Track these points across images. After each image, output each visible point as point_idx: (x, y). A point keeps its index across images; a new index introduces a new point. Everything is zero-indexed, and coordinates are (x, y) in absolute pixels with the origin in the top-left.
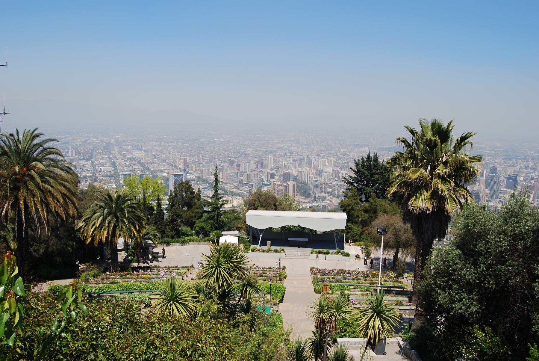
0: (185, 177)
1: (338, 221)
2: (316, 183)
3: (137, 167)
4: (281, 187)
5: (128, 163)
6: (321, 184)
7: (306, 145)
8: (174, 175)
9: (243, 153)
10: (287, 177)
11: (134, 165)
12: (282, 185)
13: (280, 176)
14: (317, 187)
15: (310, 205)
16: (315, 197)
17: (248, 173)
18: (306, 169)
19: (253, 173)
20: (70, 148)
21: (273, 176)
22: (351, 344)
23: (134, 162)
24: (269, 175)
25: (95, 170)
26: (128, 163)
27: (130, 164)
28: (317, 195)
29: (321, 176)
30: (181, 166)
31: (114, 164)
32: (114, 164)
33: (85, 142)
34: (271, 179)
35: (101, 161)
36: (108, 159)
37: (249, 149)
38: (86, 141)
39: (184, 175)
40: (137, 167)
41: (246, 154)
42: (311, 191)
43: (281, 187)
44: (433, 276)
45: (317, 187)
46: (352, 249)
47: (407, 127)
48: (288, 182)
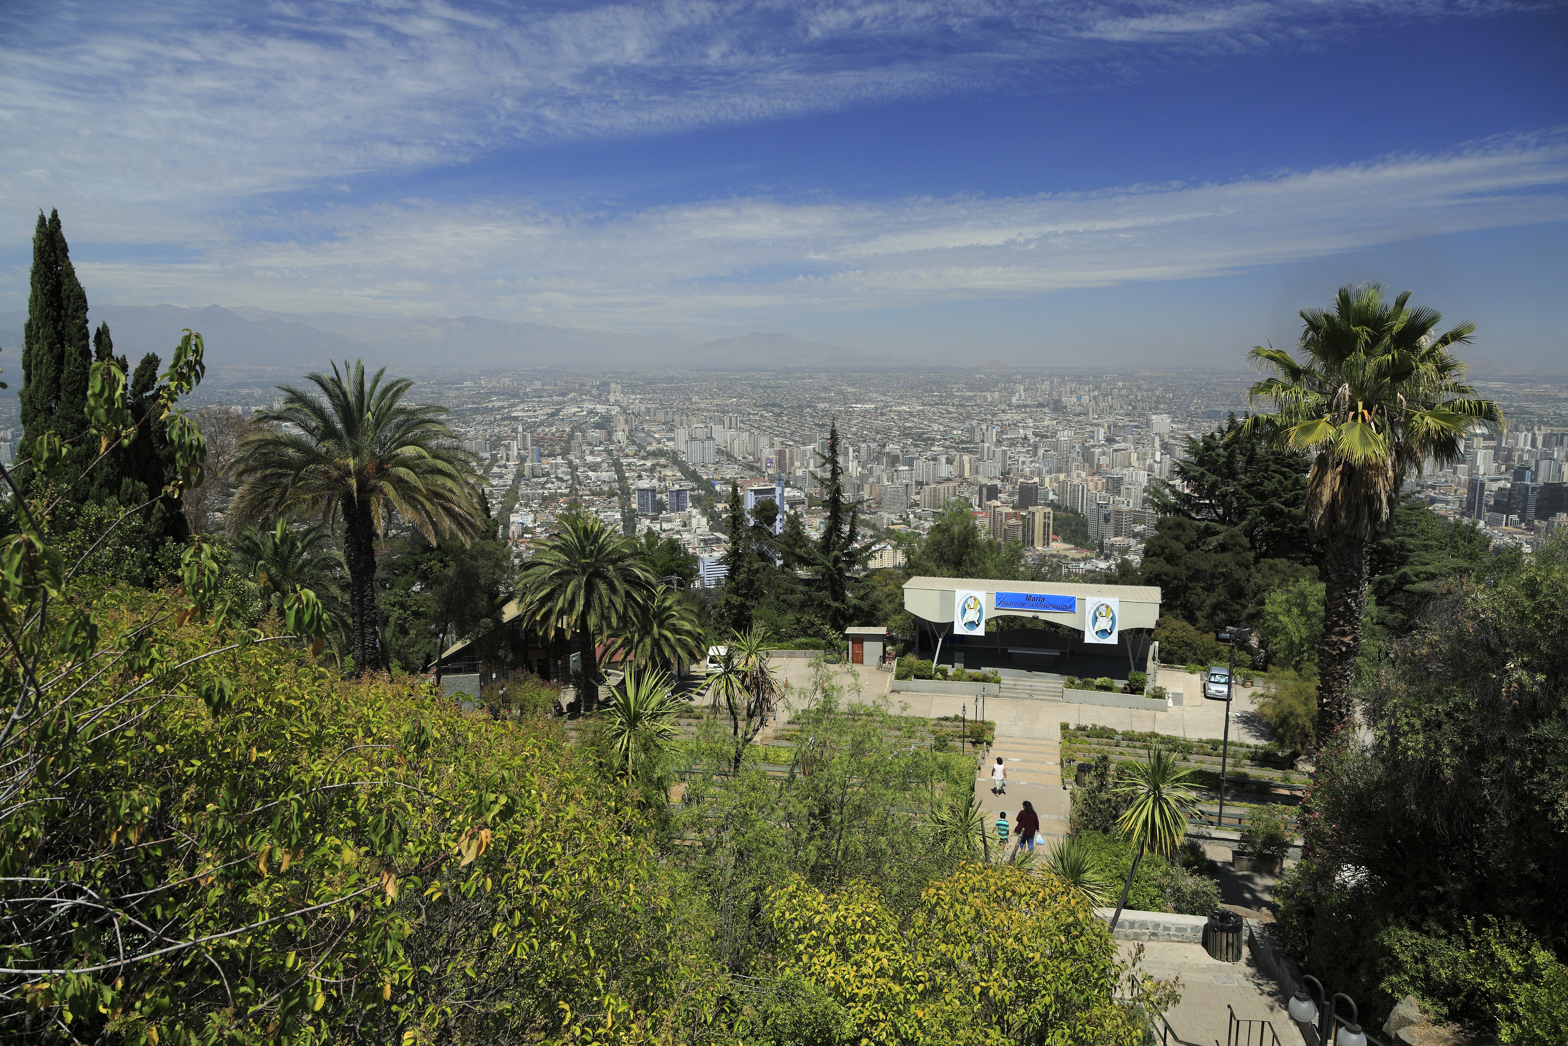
0: (782, 495)
1: (1141, 607)
2: (1104, 511)
3: (669, 473)
4: (1013, 521)
5: (649, 463)
6: (1119, 513)
7: (1079, 415)
8: (756, 492)
9: (919, 437)
10: (1028, 496)
11: (665, 466)
12: (1015, 515)
13: (1011, 494)
14: (1107, 519)
15: (1088, 566)
16: (1101, 546)
17: (933, 486)
18: (1079, 476)
19: (946, 485)
20: (520, 429)
21: (993, 492)
22: (1166, 928)
23: (663, 461)
24: (985, 491)
25: (575, 478)
26: (649, 463)
27: (654, 467)
28: (1106, 541)
29: (1119, 493)
30: (771, 471)
31: (617, 466)
32: (617, 466)
33: (553, 415)
34: (989, 499)
35: (589, 459)
36: (605, 455)
37: (935, 427)
38: (558, 411)
39: (778, 491)
40: (669, 473)
41: (929, 439)
42: (1092, 531)
43: (1013, 521)
44: (543, 972)
45: (1107, 519)
46: (1180, 683)
47: (51, 245)
48: (1031, 509)
